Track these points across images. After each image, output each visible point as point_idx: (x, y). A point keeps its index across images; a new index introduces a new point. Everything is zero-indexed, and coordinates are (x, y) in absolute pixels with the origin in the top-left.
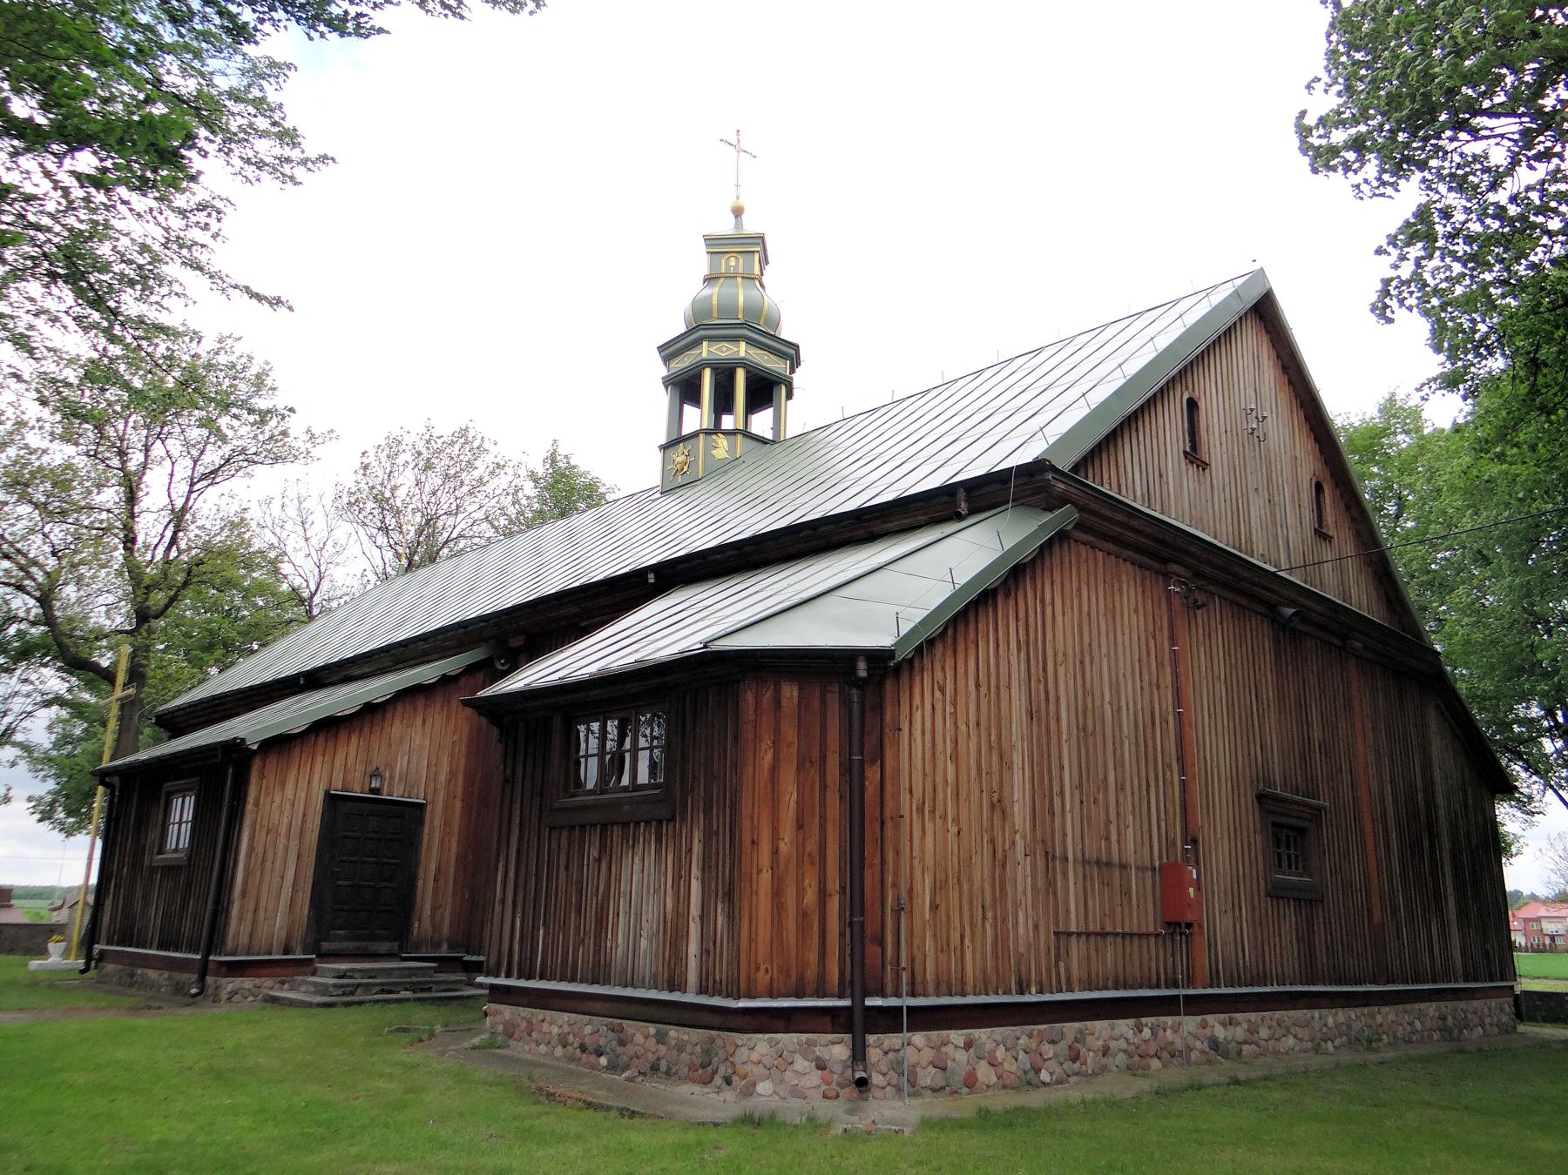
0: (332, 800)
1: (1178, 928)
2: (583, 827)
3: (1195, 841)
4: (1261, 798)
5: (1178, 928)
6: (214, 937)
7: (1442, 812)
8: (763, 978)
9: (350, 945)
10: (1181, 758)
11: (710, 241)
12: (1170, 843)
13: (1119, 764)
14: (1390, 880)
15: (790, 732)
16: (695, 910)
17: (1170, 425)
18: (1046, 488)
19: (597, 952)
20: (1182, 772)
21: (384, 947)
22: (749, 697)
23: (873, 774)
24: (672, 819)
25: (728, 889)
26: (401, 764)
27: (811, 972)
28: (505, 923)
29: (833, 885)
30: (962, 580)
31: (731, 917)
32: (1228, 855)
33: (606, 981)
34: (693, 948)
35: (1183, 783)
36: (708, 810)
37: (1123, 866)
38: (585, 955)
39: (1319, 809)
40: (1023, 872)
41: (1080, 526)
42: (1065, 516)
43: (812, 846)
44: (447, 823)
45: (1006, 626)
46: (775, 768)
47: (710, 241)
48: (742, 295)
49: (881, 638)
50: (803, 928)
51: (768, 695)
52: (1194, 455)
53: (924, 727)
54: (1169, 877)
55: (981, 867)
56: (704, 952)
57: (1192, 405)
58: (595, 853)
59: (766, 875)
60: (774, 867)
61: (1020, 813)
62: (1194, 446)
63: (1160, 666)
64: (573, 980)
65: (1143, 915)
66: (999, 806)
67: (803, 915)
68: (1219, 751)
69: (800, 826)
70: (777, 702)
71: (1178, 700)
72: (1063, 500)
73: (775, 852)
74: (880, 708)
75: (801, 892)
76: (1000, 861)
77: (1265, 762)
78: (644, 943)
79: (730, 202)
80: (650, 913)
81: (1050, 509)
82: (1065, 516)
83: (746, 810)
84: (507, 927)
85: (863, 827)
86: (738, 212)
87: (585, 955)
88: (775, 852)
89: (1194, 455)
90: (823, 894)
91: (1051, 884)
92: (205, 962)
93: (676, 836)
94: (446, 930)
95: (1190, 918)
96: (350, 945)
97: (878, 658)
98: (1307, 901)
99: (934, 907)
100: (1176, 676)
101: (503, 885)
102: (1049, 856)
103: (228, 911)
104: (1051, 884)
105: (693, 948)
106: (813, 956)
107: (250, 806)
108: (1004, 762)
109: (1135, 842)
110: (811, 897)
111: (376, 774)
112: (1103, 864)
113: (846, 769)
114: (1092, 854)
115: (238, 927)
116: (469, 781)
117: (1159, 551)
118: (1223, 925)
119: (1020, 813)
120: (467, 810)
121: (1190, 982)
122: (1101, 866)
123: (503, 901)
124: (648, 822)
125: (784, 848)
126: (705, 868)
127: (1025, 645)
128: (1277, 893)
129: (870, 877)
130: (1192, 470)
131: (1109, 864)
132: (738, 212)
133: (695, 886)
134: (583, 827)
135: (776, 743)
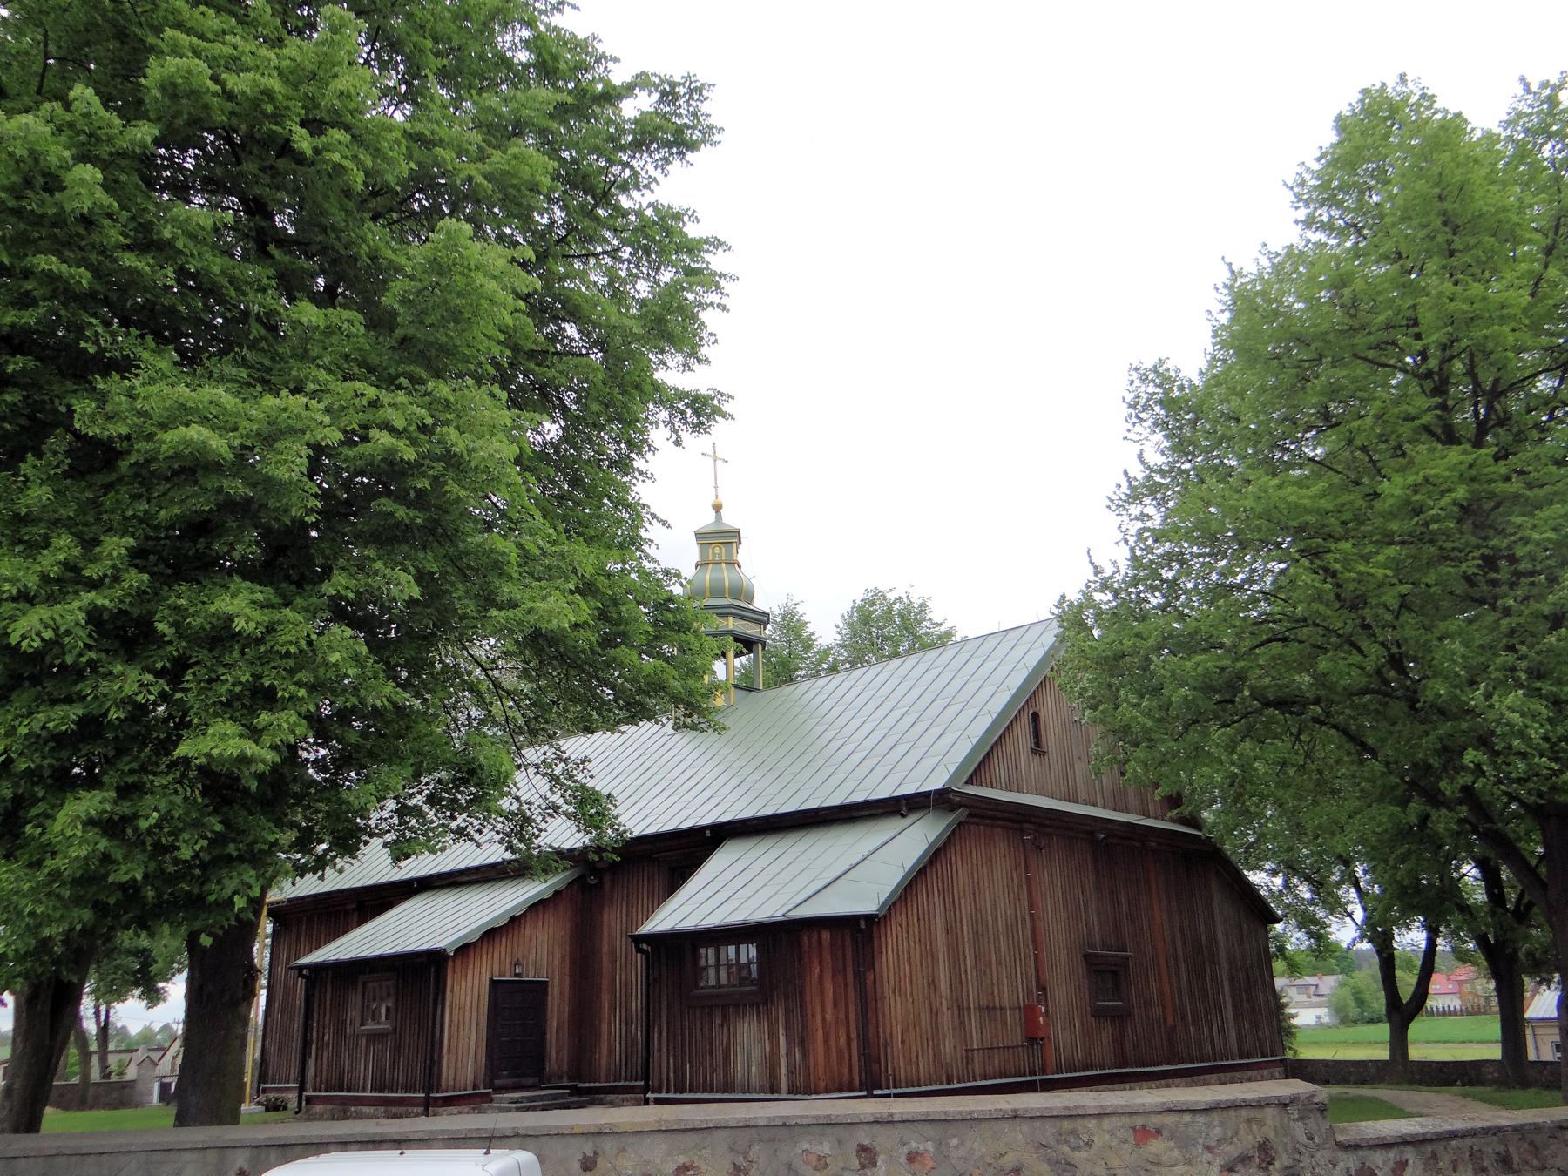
0: (494, 984)
1: (1034, 1040)
2: (710, 1007)
3: (1044, 989)
4: (1086, 956)
5: (1034, 1040)
6: (431, 1079)
7: (1221, 945)
8: (822, 1084)
9: (510, 1081)
10: (1034, 941)
11: (699, 535)
12: (1030, 992)
13: (998, 949)
14: (1180, 997)
15: (827, 957)
16: (783, 1051)
17: (1023, 737)
18: (949, 801)
19: (726, 1074)
20: (1035, 948)
21: (530, 1081)
22: (806, 939)
23: (870, 977)
24: (766, 1003)
25: (801, 1039)
26: (532, 957)
27: (845, 1079)
28: (664, 1064)
29: (854, 1035)
30: (908, 865)
31: (804, 1056)
32: (1066, 992)
33: (733, 1091)
34: (783, 1071)
35: (1036, 957)
36: (787, 998)
37: (1002, 1009)
38: (718, 1078)
39: (1127, 958)
40: (947, 1018)
41: (970, 815)
42: (961, 813)
43: (842, 1016)
44: (562, 993)
45: (934, 882)
46: (821, 976)
47: (699, 535)
48: (726, 576)
49: (869, 906)
50: (840, 1057)
51: (815, 938)
52: (1038, 748)
53: (893, 953)
54: (1029, 1013)
55: (925, 1017)
56: (790, 1072)
57: (1035, 716)
58: (719, 1021)
59: (820, 1032)
60: (824, 1028)
61: (944, 987)
62: (1038, 743)
63: (1020, 886)
64: (711, 1091)
65: (1014, 1034)
66: (933, 984)
67: (840, 1051)
68: (1058, 931)
69: (835, 1005)
70: (820, 943)
71: (1031, 905)
72: (959, 806)
73: (824, 1019)
74: (871, 941)
75: (838, 1038)
76: (935, 1014)
77: (1089, 933)
78: (754, 1070)
79: (712, 499)
80: (756, 1055)
81: (952, 810)
82: (961, 813)
83: (808, 998)
84: (664, 1064)
85: (867, 1005)
86: (717, 508)
87: (718, 1078)
88: (824, 1019)
89: (1038, 748)
90: (849, 1039)
91: (962, 1023)
92: (428, 1098)
93: (769, 1012)
94: (565, 1068)
95: (1041, 1035)
96: (510, 1081)
97: (869, 918)
98: (1119, 1017)
99: (903, 1042)
100: (1030, 892)
101: (660, 1039)
102: (960, 1008)
103: (440, 1063)
104: (962, 1023)
105: (783, 1071)
106: (846, 1071)
107: (448, 993)
108: (935, 959)
109: (1009, 993)
110: (843, 1041)
111: (518, 963)
112: (990, 1009)
113: (857, 974)
114: (984, 1002)
115: (447, 1075)
116: (573, 962)
117: (1019, 820)
118: (1063, 1037)
119: (944, 987)
120: (573, 982)
121: (1043, 1072)
122: (990, 1010)
123: (660, 1050)
124: (751, 1005)
125: (828, 1017)
126: (787, 1028)
127: (942, 892)
128: (1098, 1014)
129: (872, 1029)
130: (1037, 759)
131: (994, 1008)
132: (717, 508)
133: (782, 1039)
134: (710, 1007)
135: (821, 963)
